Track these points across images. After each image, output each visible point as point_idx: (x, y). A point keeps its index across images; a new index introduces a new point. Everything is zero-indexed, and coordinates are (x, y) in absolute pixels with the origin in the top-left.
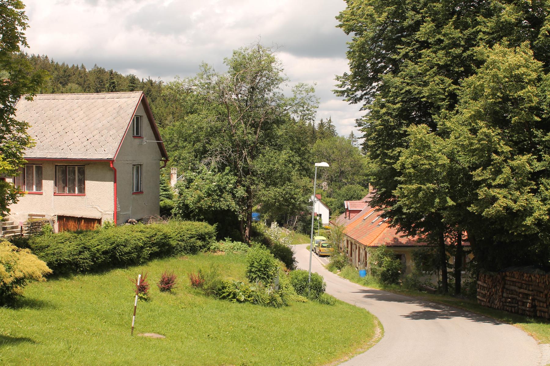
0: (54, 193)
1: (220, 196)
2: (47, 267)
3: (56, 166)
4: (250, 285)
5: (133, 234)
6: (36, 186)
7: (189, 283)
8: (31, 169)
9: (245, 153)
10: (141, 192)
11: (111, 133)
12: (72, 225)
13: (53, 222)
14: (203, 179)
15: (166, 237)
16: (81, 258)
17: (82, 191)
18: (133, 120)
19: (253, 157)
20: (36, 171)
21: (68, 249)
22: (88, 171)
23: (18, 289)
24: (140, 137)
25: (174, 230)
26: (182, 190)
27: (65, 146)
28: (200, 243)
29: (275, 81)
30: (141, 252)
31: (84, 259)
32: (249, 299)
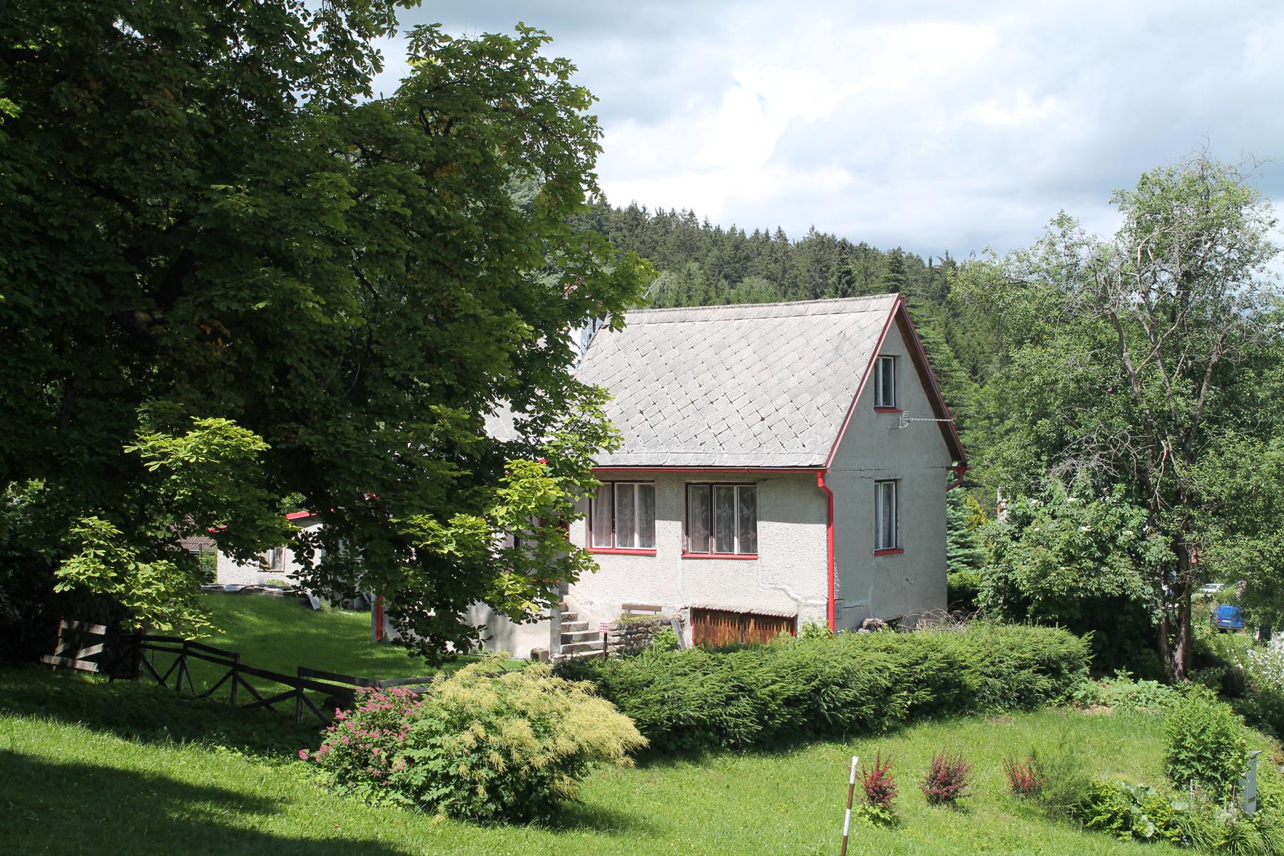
0: (684, 552)
1: (1101, 561)
2: (636, 733)
3: (687, 484)
4: (1175, 795)
5: (869, 655)
6: (641, 536)
7: (1005, 784)
8: (629, 495)
9: (1167, 445)
10: (899, 551)
11: (820, 401)
12: (725, 633)
13: (682, 623)
14: (1054, 517)
15: (951, 664)
16: (730, 715)
17: (750, 547)
18: (876, 366)
19: (1191, 458)
20: (640, 499)
21: (696, 691)
22: (764, 497)
23: (564, 783)
24: (894, 410)
25: (975, 648)
26: (1003, 544)
27: (707, 436)
28: (1044, 682)
29: (1250, 254)
30: (886, 702)
31: (737, 716)
32: (1168, 834)
